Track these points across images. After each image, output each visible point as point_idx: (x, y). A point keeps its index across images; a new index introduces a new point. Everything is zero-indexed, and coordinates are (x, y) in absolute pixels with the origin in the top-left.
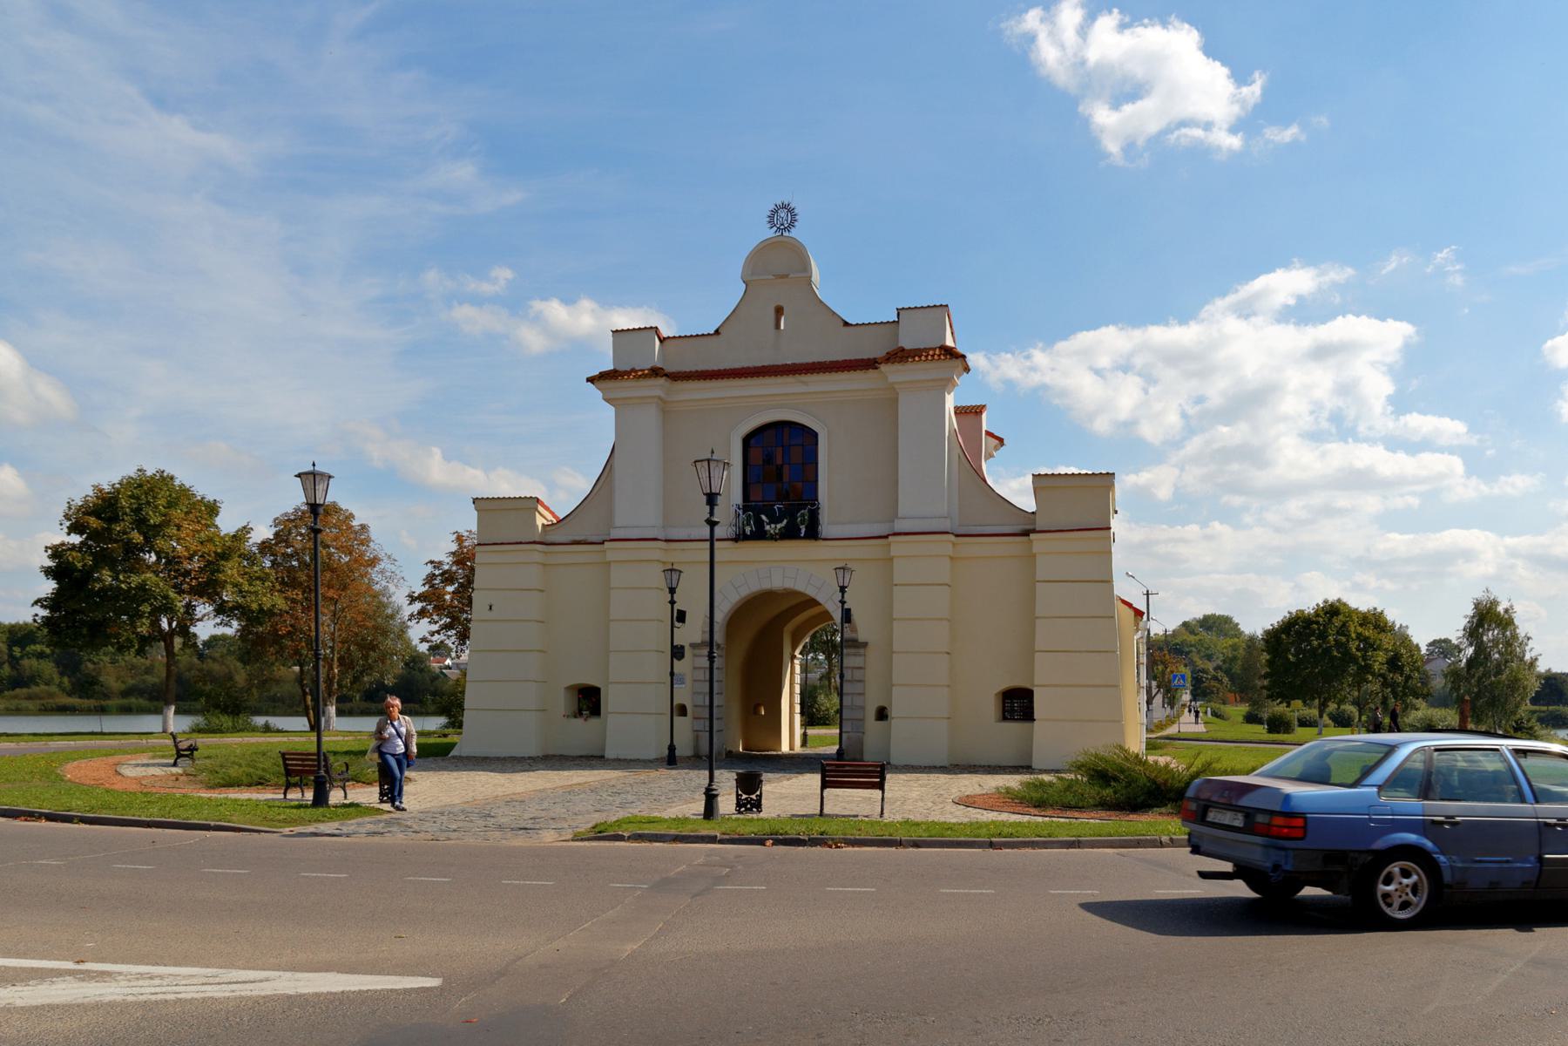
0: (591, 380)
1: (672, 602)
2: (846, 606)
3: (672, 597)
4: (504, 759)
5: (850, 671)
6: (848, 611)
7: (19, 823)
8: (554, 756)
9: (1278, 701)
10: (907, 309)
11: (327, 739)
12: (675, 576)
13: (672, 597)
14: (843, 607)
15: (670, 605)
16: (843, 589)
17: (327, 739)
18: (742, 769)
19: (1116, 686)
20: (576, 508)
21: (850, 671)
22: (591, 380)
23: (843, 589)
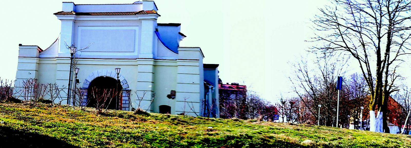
0: (55, 14)
14: (76, 79)
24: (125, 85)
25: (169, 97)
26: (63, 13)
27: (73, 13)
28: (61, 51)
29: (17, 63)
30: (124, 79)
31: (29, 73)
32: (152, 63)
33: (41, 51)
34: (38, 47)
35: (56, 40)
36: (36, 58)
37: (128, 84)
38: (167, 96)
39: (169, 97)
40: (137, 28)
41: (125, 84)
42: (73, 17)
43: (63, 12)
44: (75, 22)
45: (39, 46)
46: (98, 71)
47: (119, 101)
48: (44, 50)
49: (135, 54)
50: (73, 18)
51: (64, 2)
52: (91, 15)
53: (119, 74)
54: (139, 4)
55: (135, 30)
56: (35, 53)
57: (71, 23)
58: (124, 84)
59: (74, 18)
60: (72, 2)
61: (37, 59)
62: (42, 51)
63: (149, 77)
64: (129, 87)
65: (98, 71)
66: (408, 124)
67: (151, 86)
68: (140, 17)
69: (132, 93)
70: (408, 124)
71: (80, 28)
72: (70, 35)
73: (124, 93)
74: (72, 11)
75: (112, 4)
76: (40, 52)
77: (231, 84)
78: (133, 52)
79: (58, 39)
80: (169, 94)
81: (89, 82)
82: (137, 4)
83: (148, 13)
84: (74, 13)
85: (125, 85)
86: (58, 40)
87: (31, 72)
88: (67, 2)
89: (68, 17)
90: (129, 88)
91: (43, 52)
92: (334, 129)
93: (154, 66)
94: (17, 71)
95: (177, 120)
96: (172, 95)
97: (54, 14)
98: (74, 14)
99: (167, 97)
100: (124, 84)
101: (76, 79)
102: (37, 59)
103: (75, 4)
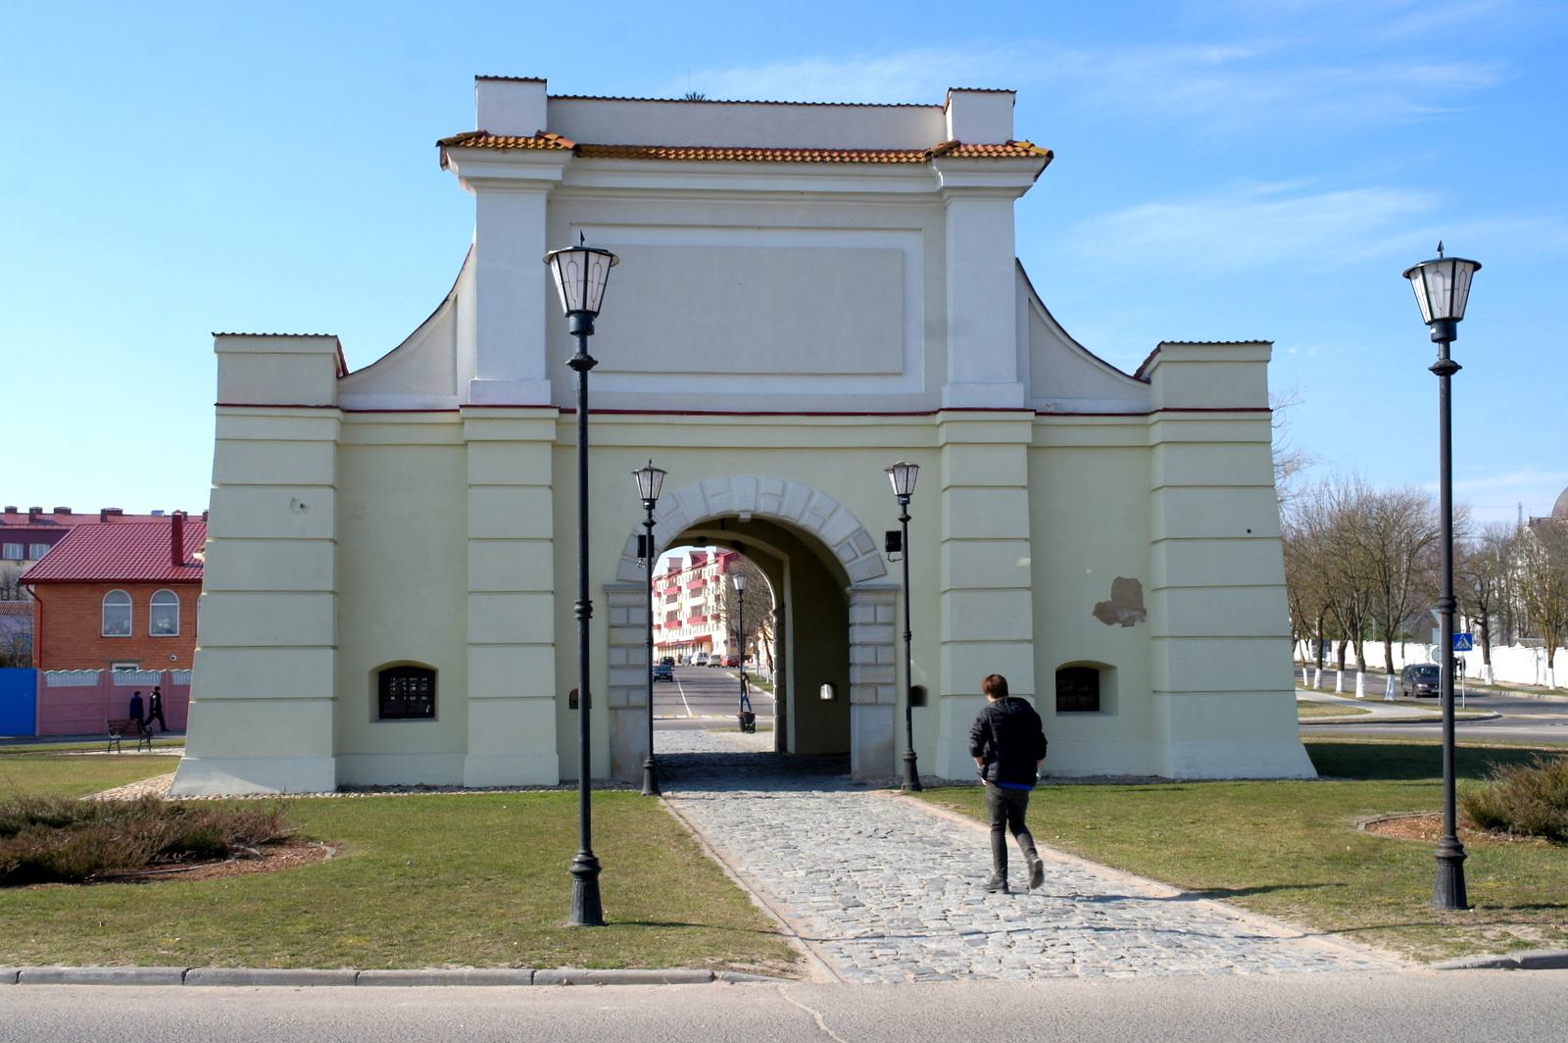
24: (862, 558)
25: (1105, 613)
27: (557, 145)
29: (214, 441)
30: (858, 529)
31: (293, 500)
32: (1024, 433)
39: (1105, 613)
40: (912, 244)
41: (864, 554)
42: (551, 168)
47: (411, 679)
49: (911, 388)
50: (556, 174)
51: (522, 76)
52: (656, 157)
57: (537, 204)
58: (857, 557)
63: (1015, 513)
64: (885, 570)
67: (1026, 561)
68: (942, 176)
73: (864, 605)
77: (52, 512)
78: (900, 374)
79: (452, 298)
80: (1106, 596)
85: (862, 558)
86: (449, 306)
87: (304, 496)
88: (506, 79)
92: (1393, 918)
94: (212, 490)
95: (855, 782)
99: (1094, 617)
100: (859, 554)
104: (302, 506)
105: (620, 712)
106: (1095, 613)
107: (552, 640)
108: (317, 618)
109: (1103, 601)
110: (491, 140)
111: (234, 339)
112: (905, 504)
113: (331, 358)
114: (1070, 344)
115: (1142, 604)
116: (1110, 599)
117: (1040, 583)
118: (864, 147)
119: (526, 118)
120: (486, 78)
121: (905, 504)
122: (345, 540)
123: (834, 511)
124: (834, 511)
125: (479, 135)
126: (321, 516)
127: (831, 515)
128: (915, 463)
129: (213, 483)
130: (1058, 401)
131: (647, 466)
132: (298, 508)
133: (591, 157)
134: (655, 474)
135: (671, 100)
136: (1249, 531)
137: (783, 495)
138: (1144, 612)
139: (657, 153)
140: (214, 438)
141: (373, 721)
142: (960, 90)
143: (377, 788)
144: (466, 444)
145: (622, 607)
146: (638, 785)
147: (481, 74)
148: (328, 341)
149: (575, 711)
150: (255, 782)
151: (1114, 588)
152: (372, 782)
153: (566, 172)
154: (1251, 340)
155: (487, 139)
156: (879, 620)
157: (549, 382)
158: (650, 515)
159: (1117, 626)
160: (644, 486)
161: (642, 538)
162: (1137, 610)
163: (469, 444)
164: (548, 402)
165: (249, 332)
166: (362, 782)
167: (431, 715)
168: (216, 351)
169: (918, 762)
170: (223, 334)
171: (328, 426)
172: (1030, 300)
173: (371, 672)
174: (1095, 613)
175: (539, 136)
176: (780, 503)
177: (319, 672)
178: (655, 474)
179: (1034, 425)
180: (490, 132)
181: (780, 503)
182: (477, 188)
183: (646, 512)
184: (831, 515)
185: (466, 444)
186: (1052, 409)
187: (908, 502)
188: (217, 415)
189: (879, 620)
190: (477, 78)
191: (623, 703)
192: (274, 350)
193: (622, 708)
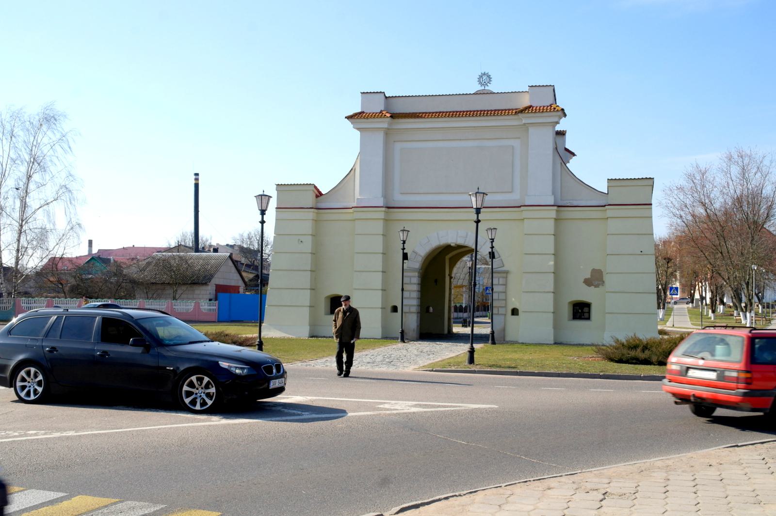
0: (348, 118)
1: (404, 249)
2: (405, 251)
3: (263, 218)
4: (536, 344)
5: (497, 294)
6: (407, 254)
7: (680, 326)
8: (533, 344)
9: (599, 356)
10: (648, 178)
11: (214, 308)
12: (265, 200)
13: (263, 218)
14: (403, 251)
15: (260, 225)
16: (404, 242)
17: (214, 308)
18: (497, 405)
19: (657, 314)
20: (587, 185)
21: (497, 294)
22: (348, 118)
23: (492, 240)
25: (588, 282)
26: (365, 116)
27: (385, 115)
28: (360, 194)
31: (299, 240)
33: (319, 194)
34: (315, 187)
35: (350, 171)
36: (313, 210)
37: (501, 260)
38: (583, 280)
39: (588, 282)
40: (516, 143)
42: (384, 123)
43: (363, 112)
44: (387, 133)
45: (316, 185)
46: (438, 234)
48: (323, 193)
49: (514, 197)
50: (386, 126)
52: (421, 117)
53: (495, 240)
54: (484, 93)
55: (513, 146)
56: (309, 200)
59: (388, 124)
60: (381, 92)
61: (313, 212)
62: (321, 194)
63: (549, 245)
65: (438, 234)
66: (464, 289)
67: (552, 263)
68: (525, 119)
69: (511, 277)
70: (464, 289)
71: (398, 146)
72: (379, 160)
74: (383, 109)
75: (547, 86)
76: (317, 196)
80: (588, 276)
81: (421, 256)
82: (480, 94)
83: (542, 110)
84: (388, 115)
86: (353, 171)
89: (407, 122)
90: (503, 266)
91: (322, 197)
93: (386, 220)
94: (274, 236)
96: (595, 279)
97: (346, 117)
98: (387, 117)
101: (403, 251)
102: (313, 212)
103: (387, 96)
104: (301, 242)
105: (407, 314)
106: (584, 282)
107: (552, 290)
108: (305, 280)
109: (587, 277)
110: (534, 108)
111: (298, 186)
112: (492, 242)
113: (312, 191)
114: (577, 180)
115: (603, 279)
116: (590, 277)
117: (557, 273)
118: (511, 108)
119: (378, 106)
120: (364, 93)
121: (492, 242)
122: (316, 254)
123: (485, 243)
124: (485, 243)
125: (360, 113)
126: (308, 246)
127: (484, 245)
128: (495, 227)
129: (275, 234)
130: (571, 201)
131: (402, 229)
132: (300, 243)
133: (398, 118)
134: (404, 232)
135: (439, 95)
136: (641, 252)
137: (466, 237)
138: (604, 282)
139: (422, 116)
140: (653, 218)
141: (569, 320)
142: (532, 86)
143: (324, 337)
144: (607, 218)
145: (408, 277)
146: (397, 339)
147: (362, 92)
148: (310, 186)
149: (395, 314)
150: (285, 333)
151: (592, 273)
152: (323, 335)
153: (390, 124)
154: (644, 177)
155: (533, 108)
156: (500, 283)
157: (553, 196)
158: (404, 246)
159: (593, 287)
160: (402, 236)
161: (490, 253)
162: (601, 281)
163: (525, 220)
164: (553, 204)
165: (621, 178)
166: (320, 335)
167: (589, 318)
168: (276, 190)
169: (495, 334)
170: (278, 185)
171: (311, 214)
172: (561, 163)
173: (327, 297)
174: (584, 282)
175: (381, 112)
176: (465, 240)
177: (305, 298)
178: (404, 232)
179: (557, 211)
180: (365, 111)
181: (465, 240)
182: (360, 131)
183: (402, 245)
184: (484, 245)
185: (523, 220)
186: (569, 205)
187: (493, 241)
188: (276, 211)
189: (500, 283)
190: (529, 86)
191: (408, 311)
192: (614, 185)
193: (407, 313)
